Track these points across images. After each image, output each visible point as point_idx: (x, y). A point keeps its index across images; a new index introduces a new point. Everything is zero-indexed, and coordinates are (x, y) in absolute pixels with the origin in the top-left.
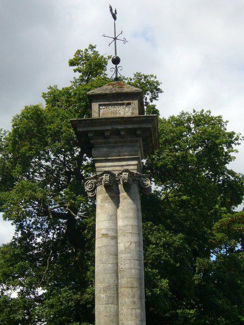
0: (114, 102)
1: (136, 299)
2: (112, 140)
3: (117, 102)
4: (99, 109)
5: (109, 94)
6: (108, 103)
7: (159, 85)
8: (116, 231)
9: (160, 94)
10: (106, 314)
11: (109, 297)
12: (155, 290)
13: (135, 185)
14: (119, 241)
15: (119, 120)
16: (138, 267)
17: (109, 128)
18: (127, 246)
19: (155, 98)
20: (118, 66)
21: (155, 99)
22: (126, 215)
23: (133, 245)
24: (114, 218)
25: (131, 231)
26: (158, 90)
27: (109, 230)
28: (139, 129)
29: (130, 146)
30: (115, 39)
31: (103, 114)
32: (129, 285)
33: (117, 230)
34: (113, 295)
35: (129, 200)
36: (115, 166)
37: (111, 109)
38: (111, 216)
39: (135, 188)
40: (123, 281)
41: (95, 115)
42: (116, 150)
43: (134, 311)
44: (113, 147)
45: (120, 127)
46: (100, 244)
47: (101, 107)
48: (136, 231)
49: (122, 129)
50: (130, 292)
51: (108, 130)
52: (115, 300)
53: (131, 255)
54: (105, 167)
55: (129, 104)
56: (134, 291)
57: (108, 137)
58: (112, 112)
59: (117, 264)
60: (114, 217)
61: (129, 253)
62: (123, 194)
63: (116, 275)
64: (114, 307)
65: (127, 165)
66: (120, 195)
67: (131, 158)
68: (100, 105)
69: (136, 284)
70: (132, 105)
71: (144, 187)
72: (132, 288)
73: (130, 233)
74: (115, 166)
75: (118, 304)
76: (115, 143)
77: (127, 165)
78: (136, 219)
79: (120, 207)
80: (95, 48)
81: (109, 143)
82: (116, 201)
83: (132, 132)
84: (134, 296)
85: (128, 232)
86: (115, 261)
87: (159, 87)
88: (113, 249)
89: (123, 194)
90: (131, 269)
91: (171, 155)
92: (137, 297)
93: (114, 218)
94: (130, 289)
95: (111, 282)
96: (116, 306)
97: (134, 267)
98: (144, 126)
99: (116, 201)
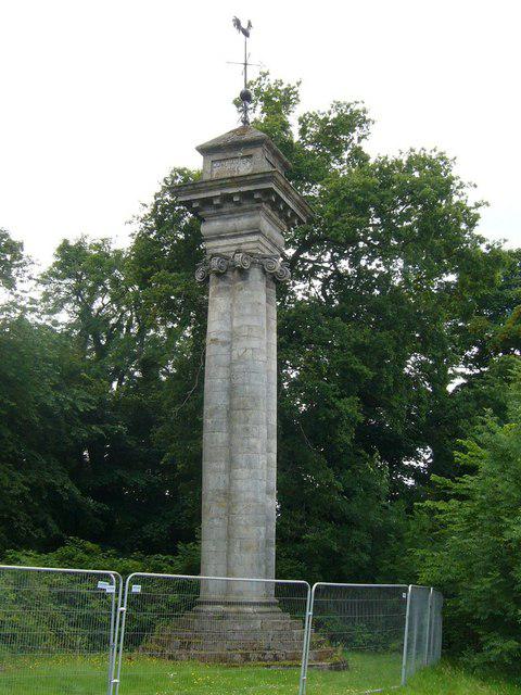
0: (232, 155)
2: (224, 210)
30: (246, 64)
45: (230, 191)
55: (250, 156)
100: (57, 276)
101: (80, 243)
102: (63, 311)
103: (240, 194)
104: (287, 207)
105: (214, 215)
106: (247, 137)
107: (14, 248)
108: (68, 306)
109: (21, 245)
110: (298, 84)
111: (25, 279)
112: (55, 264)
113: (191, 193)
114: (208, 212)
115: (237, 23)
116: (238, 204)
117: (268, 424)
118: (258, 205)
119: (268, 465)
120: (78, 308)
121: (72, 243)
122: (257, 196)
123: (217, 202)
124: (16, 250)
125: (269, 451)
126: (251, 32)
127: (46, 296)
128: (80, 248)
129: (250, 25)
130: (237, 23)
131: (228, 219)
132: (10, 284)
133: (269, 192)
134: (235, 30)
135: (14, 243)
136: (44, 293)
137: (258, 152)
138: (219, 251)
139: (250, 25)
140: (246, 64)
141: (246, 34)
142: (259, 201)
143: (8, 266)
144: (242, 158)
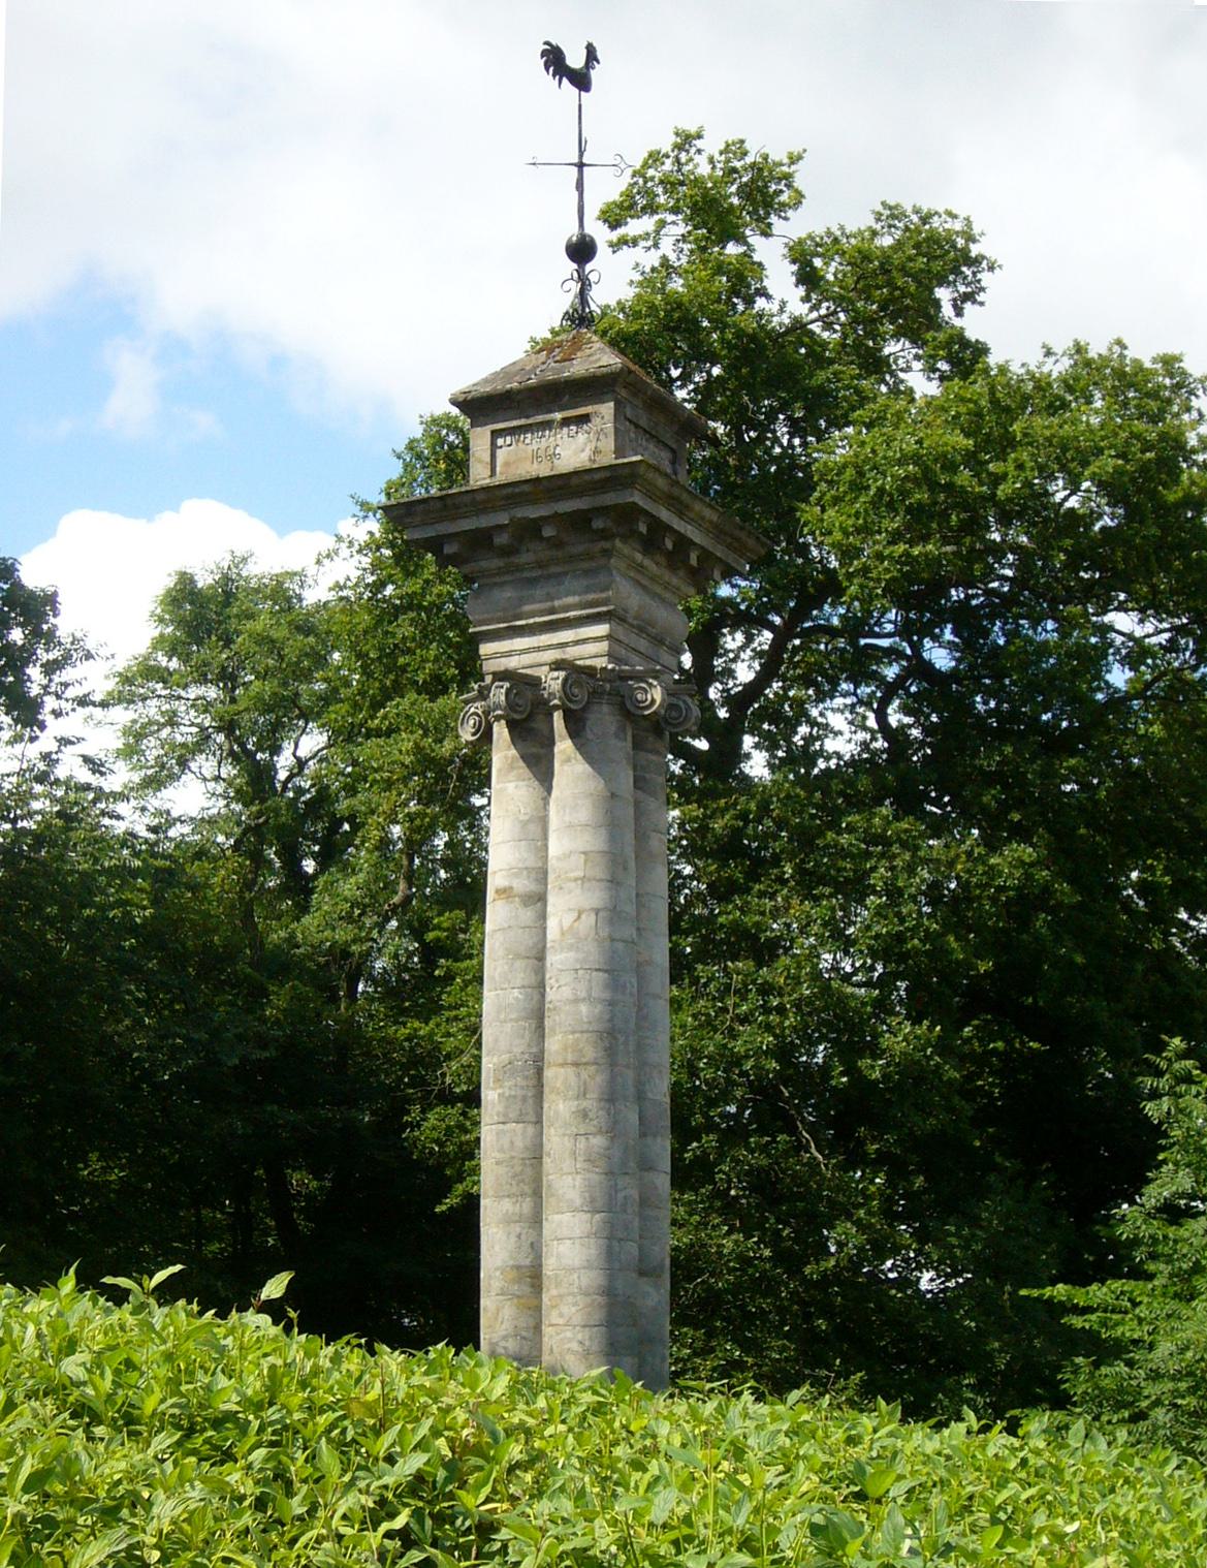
0: (540, 418)
1: (590, 1103)
2: (524, 558)
3: (530, 421)
4: (494, 447)
5: (519, 392)
6: (515, 423)
7: (974, 241)
8: (542, 875)
9: (986, 278)
10: (498, 1155)
11: (507, 1099)
12: (864, 1063)
13: (605, 708)
14: (549, 909)
15: (526, 488)
16: (607, 995)
17: (503, 518)
18: (566, 924)
19: (968, 297)
20: (588, 267)
21: (974, 302)
22: (567, 818)
23: (589, 920)
24: (537, 828)
25: (580, 874)
26: (976, 262)
27: (516, 875)
28: (603, 511)
29: (587, 573)
30: (581, 166)
31: (507, 464)
32: (570, 1058)
33: (545, 873)
34: (520, 1093)
35: (580, 767)
36: (538, 649)
37: (532, 443)
38: (524, 824)
39: (604, 718)
40: (554, 1044)
41: (479, 475)
42: (539, 592)
43: (582, 1144)
44: (532, 582)
45: (533, 512)
46: (497, 914)
47: (500, 442)
48: (599, 872)
49: (542, 518)
50: (573, 1079)
51: (500, 528)
52: (530, 1108)
53: (581, 956)
54: (509, 654)
55: (584, 419)
56: (584, 1075)
57: (508, 551)
58: (536, 456)
59: (541, 986)
60: (534, 829)
61: (571, 948)
62: (564, 746)
63: (534, 1023)
64: (524, 1132)
65: (577, 643)
66: (556, 750)
67: (599, 613)
68: (495, 434)
69: (590, 1053)
70: (596, 421)
71: (639, 712)
72: (576, 1064)
73: (576, 880)
74: (538, 649)
75: (539, 1122)
76: (540, 565)
77: (577, 643)
78: (603, 831)
79: (555, 793)
80: (699, 137)
81: (519, 568)
82: (540, 765)
83: (579, 522)
84: (582, 1094)
85: (572, 875)
86: (533, 980)
87: (975, 250)
88: (528, 940)
89: (564, 746)
90: (576, 1001)
91: (890, 557)
92: (593, 1095)
93: (537, 828)
94: (570, 1071)
95: (517, 1050)
96: (531, 1130)
97: (590, 996)
98: (610, 499)
99: (540, 765)
100: (164, 676)
101: (226, 579)
102: (187, 777)
103: (556, 517)
104: (684, 544)
105: (500, 572)
106: (578, 368)
107: (35, 608)
108: (205, 764)
109: (50, 600)
110: (794, 159)
111: (66, 706)
112: (158, 643)
113: (440, 520)
114: (484, 564)
115: (554, 59)
116: (556, 543)
117: (640, 1097)
118: (607, 545)
119: (644, 1202)
120: (228, 770)
121: (204, 580)
122: (598, 524)
123: (501, 540)
124: (42, 617)
125: (646, 1165)
126: (595, 75)
127: (136, 736)
128: (228, 591)
129: (591, 55)
130: (554, 59)
131: (557, 576)
132: (27, 713)
133: (630, 513)
134: (548, 80)
135: (32, 595)
136: (126, 732)
137: (604, 412)
138: (512, 663)
139: (591, 55)
140: (581, 166)
141: (581, 81)
142: (604, 534)
143: (19, 659)
144: (566, 422)
